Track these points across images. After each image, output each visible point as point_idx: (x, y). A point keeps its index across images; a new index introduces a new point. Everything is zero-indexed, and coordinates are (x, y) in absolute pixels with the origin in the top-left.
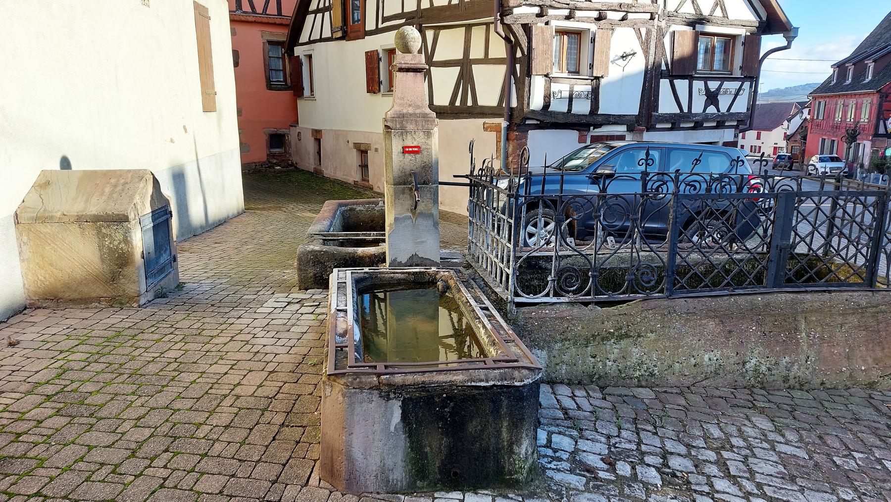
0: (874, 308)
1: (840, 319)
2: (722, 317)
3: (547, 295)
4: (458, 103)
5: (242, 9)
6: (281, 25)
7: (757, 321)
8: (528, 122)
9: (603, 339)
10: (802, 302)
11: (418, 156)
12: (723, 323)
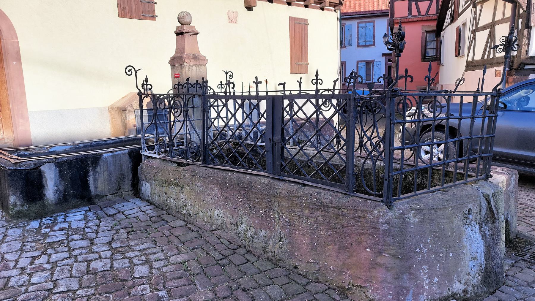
0: (337, 210)
1: (307, 212)
2: (223, 185)
3: (155, 153)
4: (486, 57)
5: (412, 15)
6: (432, 20)
7: (244, 195)
8: (527, 67)
9: (169, 184)
10: (275, 187)
11: (179, 79)
12: (222, 190)
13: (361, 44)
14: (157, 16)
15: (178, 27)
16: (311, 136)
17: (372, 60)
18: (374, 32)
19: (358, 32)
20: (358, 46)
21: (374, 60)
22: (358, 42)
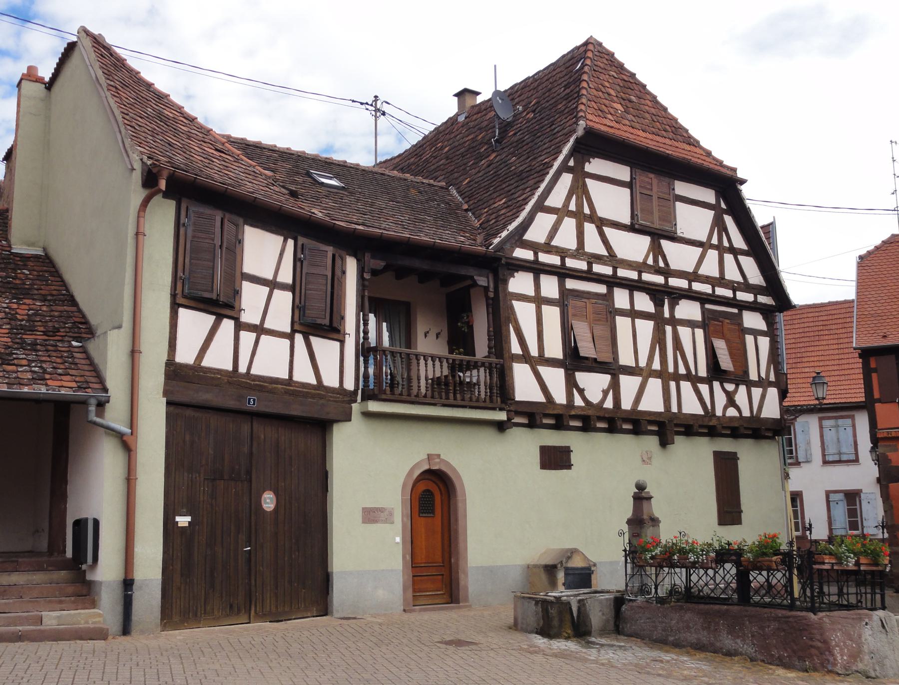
13: (830, 458)
14: (572, 451)
15: (635, 493)
16: (184, 225)
17: (858, 490)
18: (855, 436)
19: (822, 436)
20: (825, 462)
21: (861, 491)
22: (824, 455)
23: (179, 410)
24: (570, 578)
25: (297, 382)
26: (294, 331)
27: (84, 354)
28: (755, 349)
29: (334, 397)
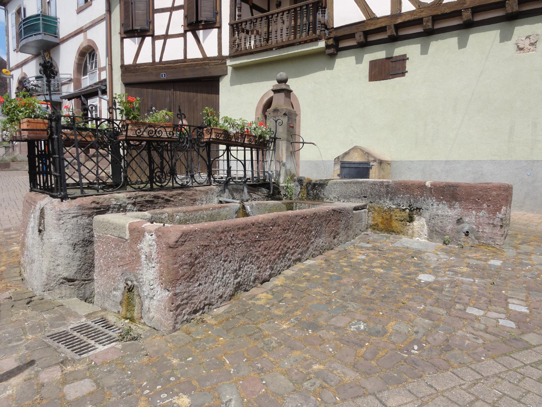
23: (134, 90)
24: (346, 171)
25: (189, 59)
26: (186, 31)
27: (285, 13)
28: (161, 50)
29: (214, 63)
